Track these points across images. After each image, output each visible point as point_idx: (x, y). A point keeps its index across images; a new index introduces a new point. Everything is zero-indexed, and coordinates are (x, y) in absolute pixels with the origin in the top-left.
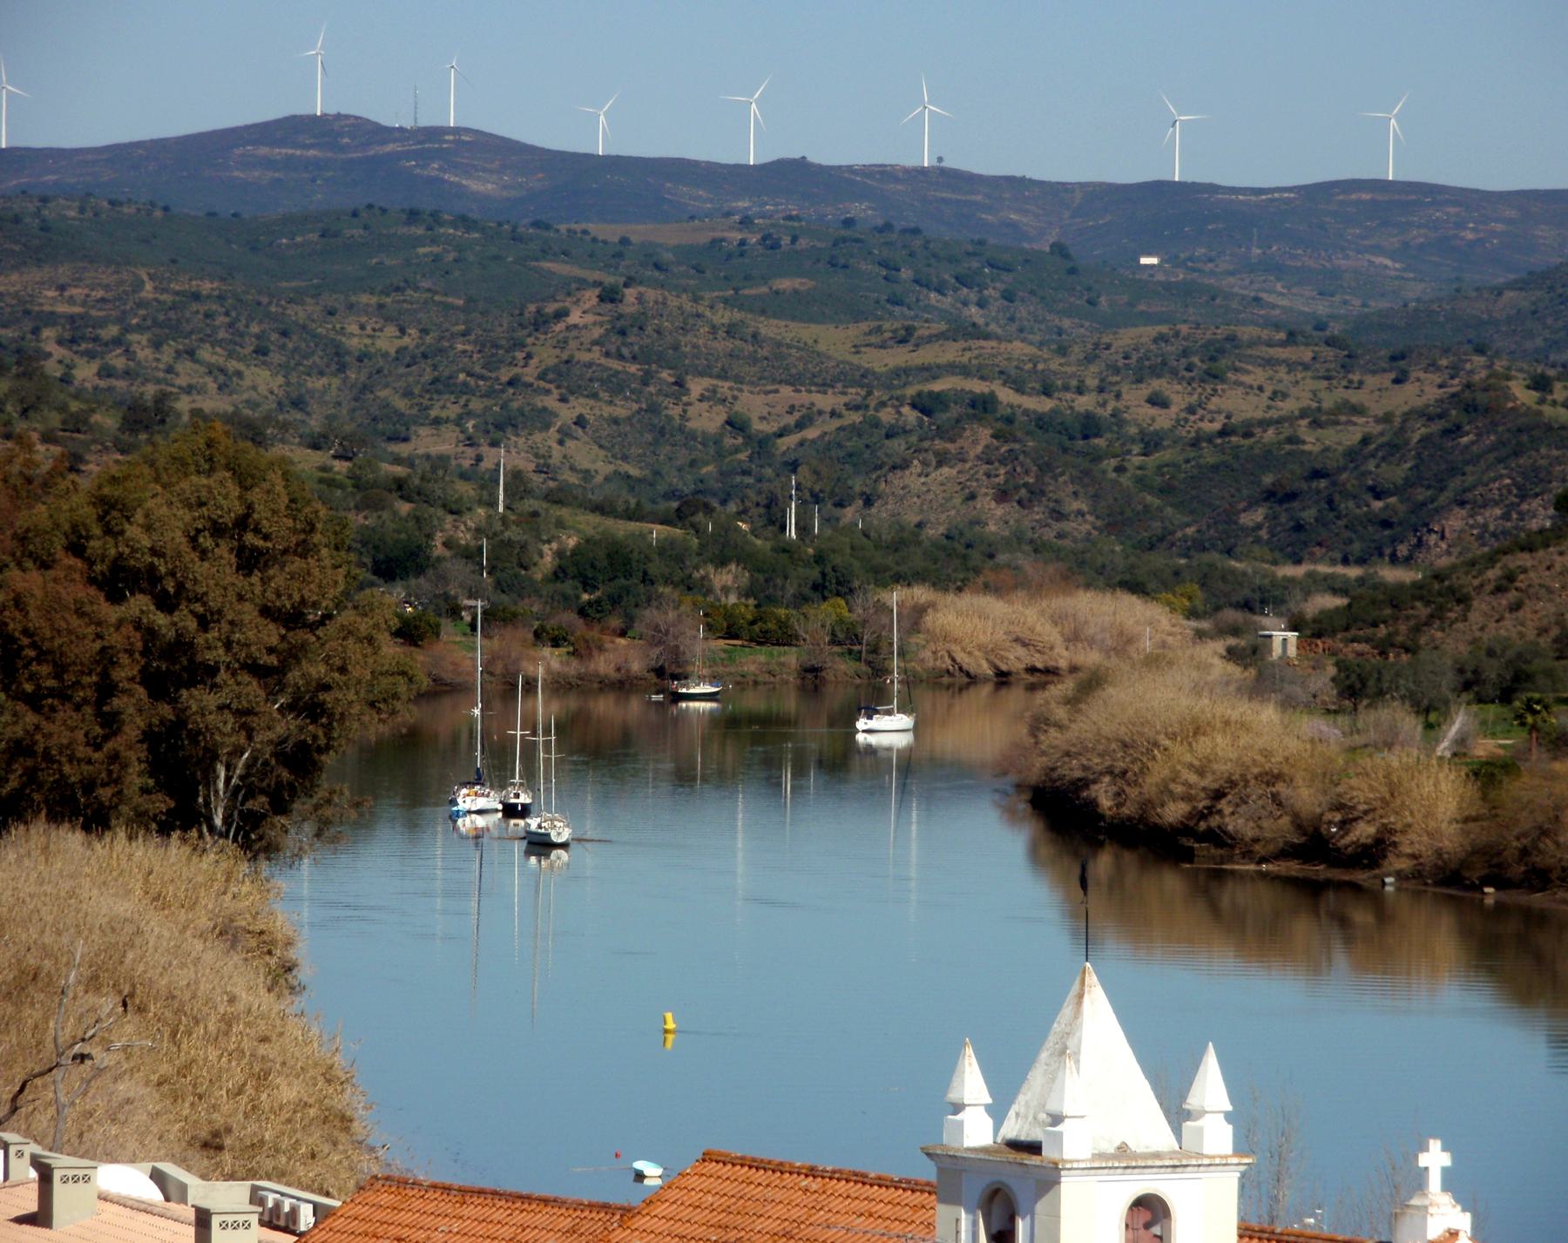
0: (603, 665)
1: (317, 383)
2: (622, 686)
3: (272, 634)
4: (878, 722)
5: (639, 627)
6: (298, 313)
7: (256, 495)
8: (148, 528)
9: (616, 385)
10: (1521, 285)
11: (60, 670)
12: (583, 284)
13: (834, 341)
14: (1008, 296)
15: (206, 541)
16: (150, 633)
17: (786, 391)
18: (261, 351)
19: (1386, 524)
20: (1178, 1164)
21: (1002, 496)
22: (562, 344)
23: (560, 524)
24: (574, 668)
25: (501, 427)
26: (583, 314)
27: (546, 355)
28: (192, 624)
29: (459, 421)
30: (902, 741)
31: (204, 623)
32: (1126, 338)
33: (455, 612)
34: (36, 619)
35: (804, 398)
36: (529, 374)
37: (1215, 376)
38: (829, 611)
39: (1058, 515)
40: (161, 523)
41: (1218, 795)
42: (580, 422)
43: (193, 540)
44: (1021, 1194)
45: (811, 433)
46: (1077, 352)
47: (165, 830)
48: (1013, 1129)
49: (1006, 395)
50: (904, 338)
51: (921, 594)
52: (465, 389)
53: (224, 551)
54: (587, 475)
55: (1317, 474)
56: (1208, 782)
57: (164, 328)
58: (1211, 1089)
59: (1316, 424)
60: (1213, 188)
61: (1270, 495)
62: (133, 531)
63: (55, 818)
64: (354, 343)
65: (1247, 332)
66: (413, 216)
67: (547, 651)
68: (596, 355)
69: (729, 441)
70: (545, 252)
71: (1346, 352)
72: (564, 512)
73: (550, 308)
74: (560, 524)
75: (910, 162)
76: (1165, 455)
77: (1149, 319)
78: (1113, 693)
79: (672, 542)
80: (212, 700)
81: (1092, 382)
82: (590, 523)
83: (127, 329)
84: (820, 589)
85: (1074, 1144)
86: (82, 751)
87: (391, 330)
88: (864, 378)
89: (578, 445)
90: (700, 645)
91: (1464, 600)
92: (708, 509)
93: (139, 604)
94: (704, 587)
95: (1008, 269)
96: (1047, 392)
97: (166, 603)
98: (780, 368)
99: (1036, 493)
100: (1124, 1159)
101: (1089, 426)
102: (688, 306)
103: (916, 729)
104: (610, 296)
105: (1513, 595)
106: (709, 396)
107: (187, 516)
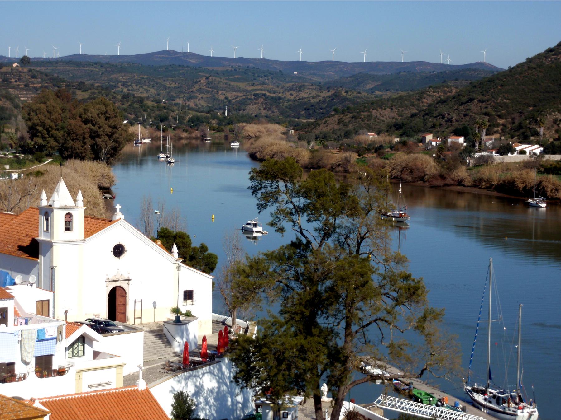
0: (193, 135)
1: (161, 92)
2: (196, 138)
3: (110, 130)
4: (234, 144)
5: (199, 130)
6: (159, 81)
7: (108, 108)
8: (91, 113)
9: (208, 92)
10: (350, 77)
11: (77, 136)
12: (203, 76)
13: (242, 85)
14: (272, 78)
15: (100, 115)
16: (91, 129)
17: (234, 93)
18: (153, 87)
19: (323, 114)
20: (73, 208)
21: (265, 109)
22: (200, 85)
23: (189, 113)
24: (189, 135)
25: (189, 98)
26: (203, 81)
27: (197, 87)
28: (98, 128)
29: (183, 98)
30: (238, 147)
31: (100, 128)
32: (288, 85)
33: (171, 127)
34: (73, 127)
35: (237, 94)
36: (194, 90)
37: (300, 91)
38: (229, 127)
39: (273, 112)
40: (93, 113)
41: (274, 155)
42: (202, 98)
43: (98, 115)
44: (49, 212)
45: (238, 100)
46: (280, 87)
47: (94, 160)
48: (50, 203)
49: (268, 94)
50: (253, 85)
51: (244, 124)
52: (184, 93)
53: (103, 117)
54: (203, 106)
55: (312, 106)
56: (273, 153)
57: (138, 83)
58: (80, 196)
59: (313, 98)
60: (306, 62)
61: (305, 109)
62: (88, 114)
63: (75, 158)
64: (168, 86)
65: (306, 84)
66: (180, 66)
67: (185, 133)
68: (205, 87)
69: (225, 101)
70: (200, 72)
71: (320, 87)
72: (190, 112)
73: (198, 80)
74: (189, 113)
75: (259, 58)
76: (290, 103)
77: (293, 82)
78: (261, 139)
79: (206, 116)
80: (101, 140)
81: (282, 92)
82: (194, 113)
83: (132, 83)
84: (229, 124)
85: (56, 205)
86: (80, 148)
87: (174, 84)
88: (246, 91)
89: (201, 102)
90: (208, 131)
91: (319, 125)
92: (213, 111)
93: (89, 125)
94: (211, 123)
95: (272, 74)
96: (274, 93)
97: (94, 125)
98: (233, 89)
99: (270, 109)
100: (66, 207)
101: (280, 98)
102: (220, 80)
103: (240, 145)
104: (207, 78)
105: (326, 124)
106: (222, 94)
107: (97, 111)
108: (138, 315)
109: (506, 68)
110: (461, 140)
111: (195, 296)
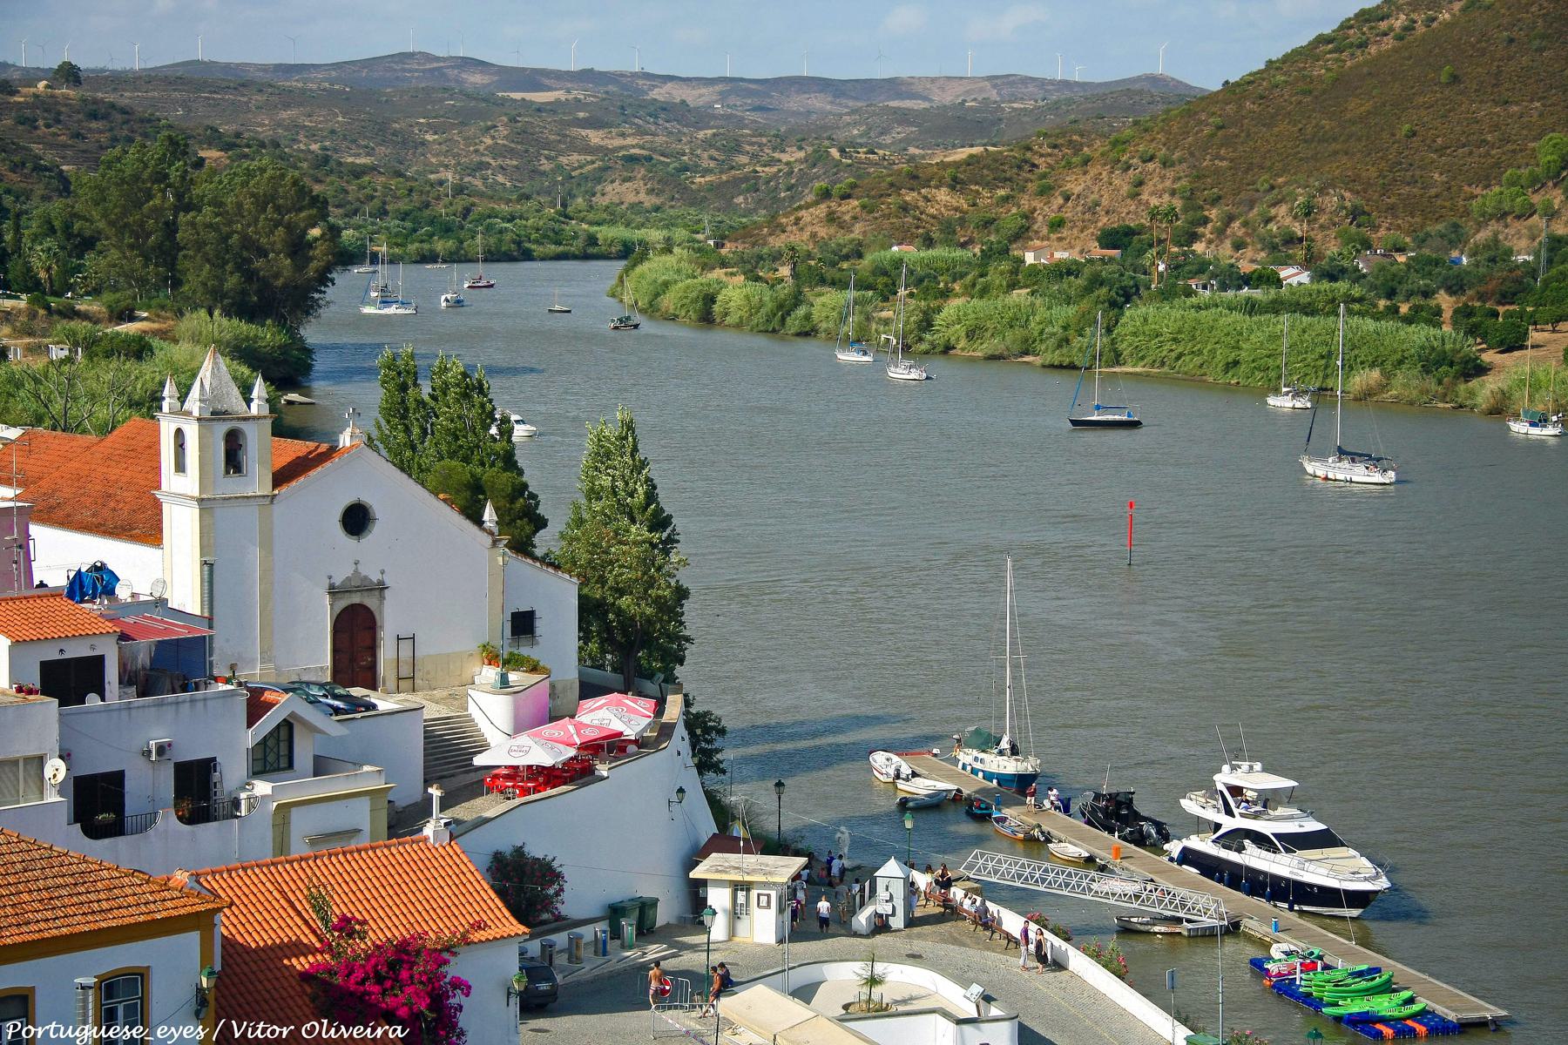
108: (405, 671)
109: (1215, 86)
110: (1030, 258)
111: (541, 626)
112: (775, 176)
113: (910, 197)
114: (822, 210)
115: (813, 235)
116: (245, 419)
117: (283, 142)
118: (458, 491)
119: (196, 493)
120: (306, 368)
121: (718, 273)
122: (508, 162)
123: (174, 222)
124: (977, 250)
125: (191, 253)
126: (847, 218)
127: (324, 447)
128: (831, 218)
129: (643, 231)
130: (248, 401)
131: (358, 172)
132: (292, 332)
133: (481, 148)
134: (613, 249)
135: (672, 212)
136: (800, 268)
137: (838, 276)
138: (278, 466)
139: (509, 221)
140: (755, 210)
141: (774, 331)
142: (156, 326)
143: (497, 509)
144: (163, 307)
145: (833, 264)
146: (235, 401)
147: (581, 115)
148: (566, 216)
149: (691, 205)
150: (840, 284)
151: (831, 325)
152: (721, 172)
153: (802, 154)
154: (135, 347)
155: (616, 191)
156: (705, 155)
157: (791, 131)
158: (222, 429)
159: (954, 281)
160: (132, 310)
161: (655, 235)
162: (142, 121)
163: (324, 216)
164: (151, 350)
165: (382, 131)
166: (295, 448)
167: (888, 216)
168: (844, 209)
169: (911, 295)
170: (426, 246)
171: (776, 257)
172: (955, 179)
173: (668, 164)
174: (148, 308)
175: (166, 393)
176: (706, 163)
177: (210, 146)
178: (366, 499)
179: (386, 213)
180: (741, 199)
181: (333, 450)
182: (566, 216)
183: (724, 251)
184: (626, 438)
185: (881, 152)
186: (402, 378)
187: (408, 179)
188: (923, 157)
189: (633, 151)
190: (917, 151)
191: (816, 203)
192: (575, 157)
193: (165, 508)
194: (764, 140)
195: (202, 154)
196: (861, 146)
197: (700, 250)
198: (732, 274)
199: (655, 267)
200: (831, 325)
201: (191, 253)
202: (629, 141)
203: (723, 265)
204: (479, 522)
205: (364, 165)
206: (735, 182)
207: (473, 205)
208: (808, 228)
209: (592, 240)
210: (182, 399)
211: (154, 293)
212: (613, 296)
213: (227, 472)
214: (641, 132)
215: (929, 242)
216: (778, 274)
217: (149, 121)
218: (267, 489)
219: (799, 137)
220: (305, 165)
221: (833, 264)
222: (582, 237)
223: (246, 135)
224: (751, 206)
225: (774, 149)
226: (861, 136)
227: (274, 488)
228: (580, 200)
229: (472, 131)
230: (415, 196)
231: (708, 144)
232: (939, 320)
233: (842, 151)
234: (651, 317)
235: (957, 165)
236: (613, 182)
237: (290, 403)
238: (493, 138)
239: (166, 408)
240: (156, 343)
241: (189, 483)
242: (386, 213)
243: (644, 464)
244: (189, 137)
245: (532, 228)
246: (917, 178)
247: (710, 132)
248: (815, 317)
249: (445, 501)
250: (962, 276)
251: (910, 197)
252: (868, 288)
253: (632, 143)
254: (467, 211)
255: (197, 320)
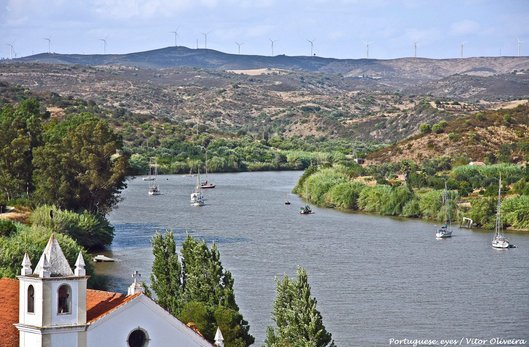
112: (396, 119)
113: (481, 132)
114: (425, 140)
115: (420, 155)
116: (71, 279)
117: (97, 102)
118: (199, 321)
119: (40, 325)
120: (109, 240)
121: (360, 179)
122: (233, 112)
123: (31, 152)
124: (524, 165)
125: (41, 171)
126: (441, 144)
127: (118, 295)
128: (431, 145)
129: (314, 153)
130: (73, 267)
131: (142, 119)
132: (101, 218)
133: (217, 104)
134: (296, 164)
135: (333, 141)
136: (412, 176)
137: (435, 180)
138: (90, 307)
139: (233, 148)
140: (384, 139)
141: (395, 214)
142: (19, 215)
143: (223, 332)
144: (23, 204)
145: (432, 173)
146: (65, 268)
147: (277, 83)
148: (267, 144)
149: (344, 136)
150: (438, 186)
151: (431, 211)
152: (363, 117)
153: (413, 105)
154: (5, 228)
155: (299, 129)
156: (353, 106)
157: (406, 91)
158: (56, 285)
159: (509, 184)
160: (4, 206)
161: (322, 155)
162: (13, 90)
163: (119, 145)
164: (15, 231)
165: (157, 94)
166: (102, 296)
167: (467, 144)
168: (439, 139)
169: (482, 193)
170: (183, 164)
171: (397, 169)
172: (509, 120)
173: (330, 112)
174: (14, 204)
175: (23, 264)
176: (353, 111)
177: (54, 104)
178: (144, 327)
179: (159, 143)
180: (374, 133)
181: (124, 297)
182: (267, 144)
183: (364, 166)
184: (302, 287)
185: (462, 104)
186: (165, 250)
187: (172, 123)
188: (489, 106)
189: (308, 104)
190: (485, 103)
191: (421, 136)
192: (273, 108)
193: (21, 334)
194: (389, 97)
195: (49, 110)
196: (450, 100)
197: (349, 165)
198: (369, 180)
199: (320, 176)
200: (431, 211)
201: (41, 171)
202: (306, 98)
203: (364, 174)
204: (211, 340)
205: (146, 115)
206: (371, 123)
207: (211, 138)
208: (417, 151)
209: (283, 159)
210: (33, 268)
211: (18, 195)
212: (296, 193)
213: (59, 312)
214: (313, 93)
215: (493, 160)
216: (398, 180)
217: (18, 90)
218: (83, 322)
219: (412, 94)
220: (110, 115)
221: (432, 173)
222: (277, 156)
223: (75, 98)
224: (381, 137)
225: (396, 102)
226: (450, 94)
227: (88, 320)
228: (276, 135)
229: (210, 93)
230: (176, 134)
231: (354, 100)
232: (500, 208)
233: (438, 103)
234: (319, 206)
235: (511, 111)
236: (296, 123)
237: (99, 261)
238: (224, 97)
239: (23, 272)
240: (18, 225)
241: (36, 319)
242: (159, 143)
243: (314, 302)
244: (38, 99)
245: (247, 151)
246: (485, 120)
247: (356, 92)
248: (421, 206)
249: (191, 327)
250: (515, 181)
251: (481, 132)
252: (454, 188)
253: (308, 100)
254: (207, 142)
255: (43, 211)
